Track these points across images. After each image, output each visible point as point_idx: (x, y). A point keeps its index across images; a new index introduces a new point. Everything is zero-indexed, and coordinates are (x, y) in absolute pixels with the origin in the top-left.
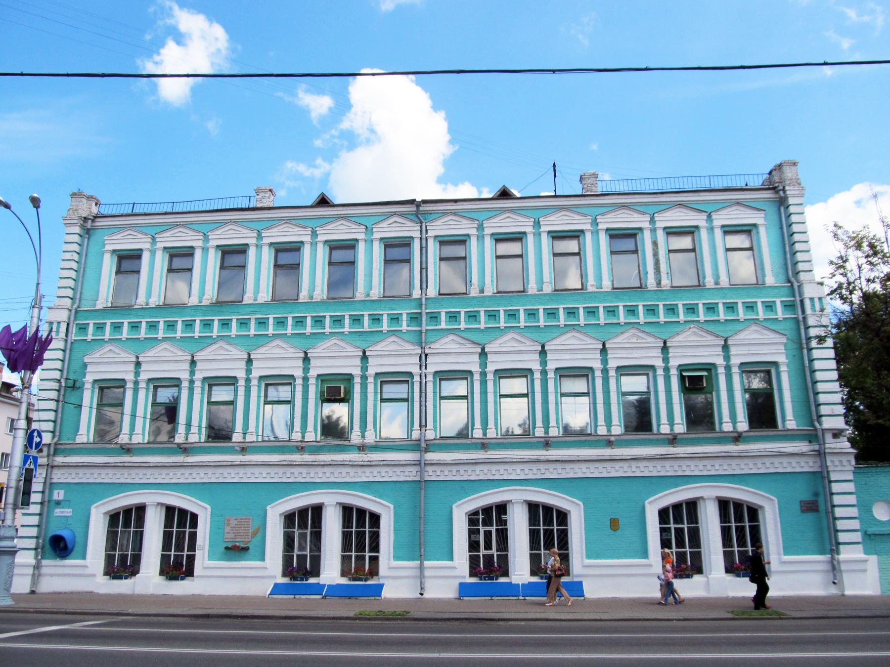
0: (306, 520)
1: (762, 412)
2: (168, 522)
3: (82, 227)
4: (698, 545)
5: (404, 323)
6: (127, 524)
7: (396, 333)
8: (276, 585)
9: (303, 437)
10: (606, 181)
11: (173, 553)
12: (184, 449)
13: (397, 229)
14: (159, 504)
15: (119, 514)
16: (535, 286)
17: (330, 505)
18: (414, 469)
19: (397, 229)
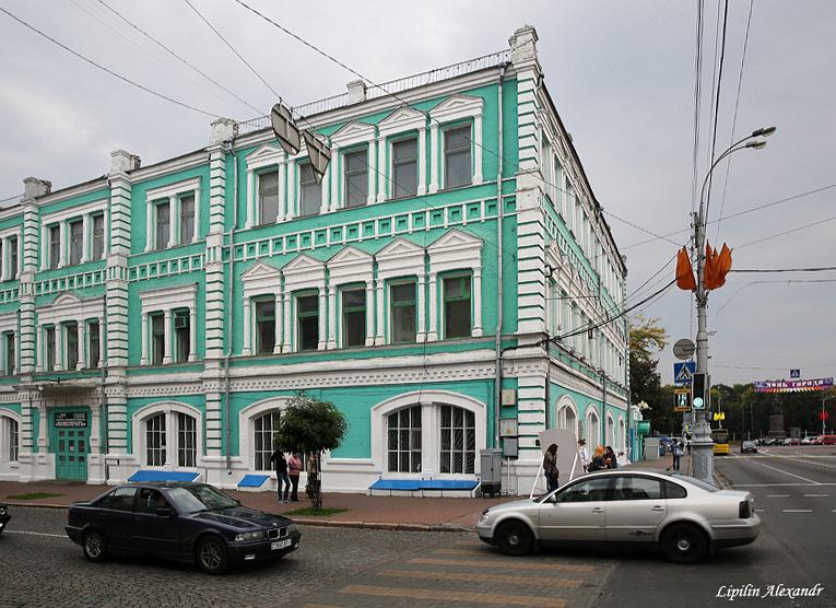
1: (457, 320)
2: (445, 422)
3: (223, 151)
4: (180, 451)
5: (446, 219)
7: (403, 236)
8: (248, 477)
10: (305, 116)
12: (426, 348)
14: (434, 403)
16: (480, 175)
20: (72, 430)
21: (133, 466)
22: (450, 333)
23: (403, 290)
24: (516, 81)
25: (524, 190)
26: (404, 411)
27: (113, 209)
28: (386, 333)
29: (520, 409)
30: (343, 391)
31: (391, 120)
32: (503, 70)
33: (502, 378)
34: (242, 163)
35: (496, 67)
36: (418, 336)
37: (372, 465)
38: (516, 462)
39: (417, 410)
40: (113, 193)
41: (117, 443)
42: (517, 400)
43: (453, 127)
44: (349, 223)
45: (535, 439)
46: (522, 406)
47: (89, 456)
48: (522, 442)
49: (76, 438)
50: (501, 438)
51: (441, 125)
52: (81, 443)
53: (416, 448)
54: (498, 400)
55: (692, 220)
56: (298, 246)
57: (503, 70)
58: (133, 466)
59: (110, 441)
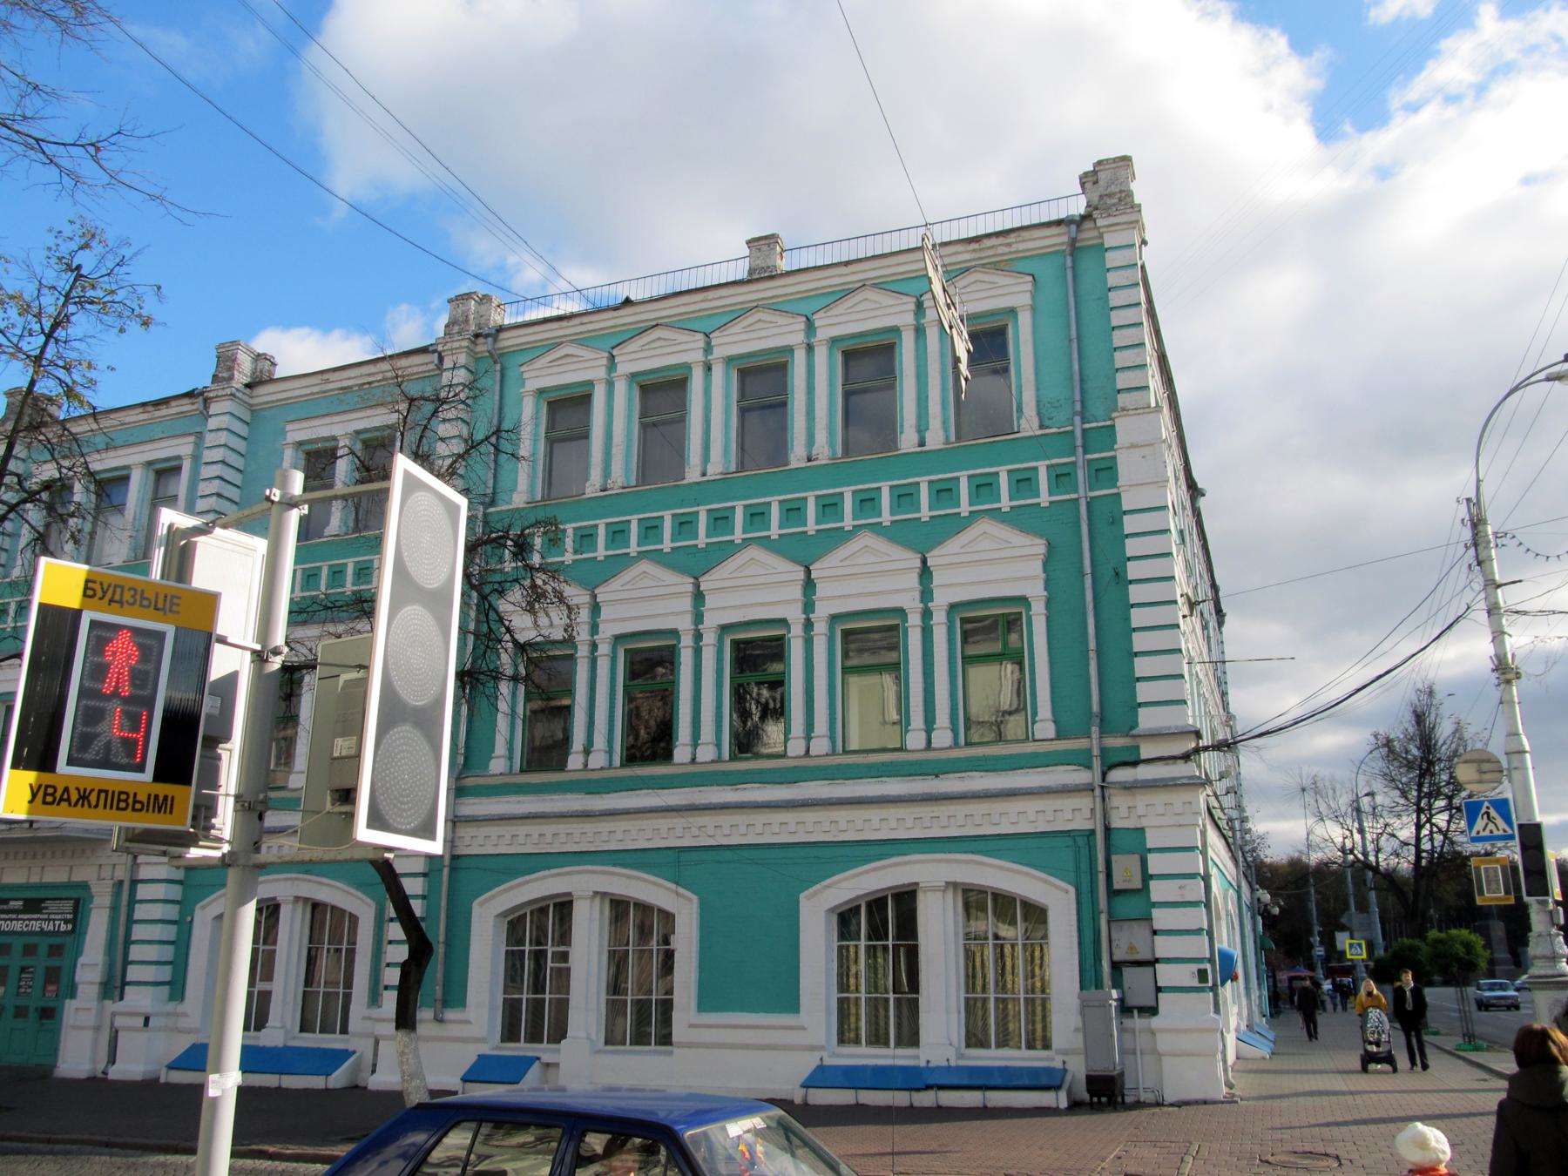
0: (888, 921)
6: (877, 932)
9: (929, 741)
11: (547, 996)
13: (763, 334)
15: (858, 908)
17: (933, 889)
18: (1084, 802)
19: (763, 334)
20: (34, 940)
21: (180, 1031)
22: (633, 756)
23: (650, 665)
24: (1102, 249)
25: (1133, 446)
26: (877, 904)
27: (209, 456)
28: (511, 749)
29: (1154, 898)
30: (728, 855)
31: (835, 311)
32: (1073, 227)
33: (1107, 829)
34: (511, 374)
35: (1059, 223)
36: (570, 758)
37: (803, 1028)
38: (1155, 1022)
39: (906, 899)
40: (213, 423)
41: (148, 974)
42: (1147, 877)
43: (753, 362)
44: (971, 472)
45: (1195, 967)
46: (1158, 891)
47: (70, 1006)
48: (1166, 974)
49: (42, 961)
50: (1116, 966)
51: (729, 360)
52: (53, 975)
53: (536, 992)
54: (1102, 878)
55: (1463, 511)
56: (323, 588)
57: (1073, 227)
58: (180, 1031)
59: (130, 968)
